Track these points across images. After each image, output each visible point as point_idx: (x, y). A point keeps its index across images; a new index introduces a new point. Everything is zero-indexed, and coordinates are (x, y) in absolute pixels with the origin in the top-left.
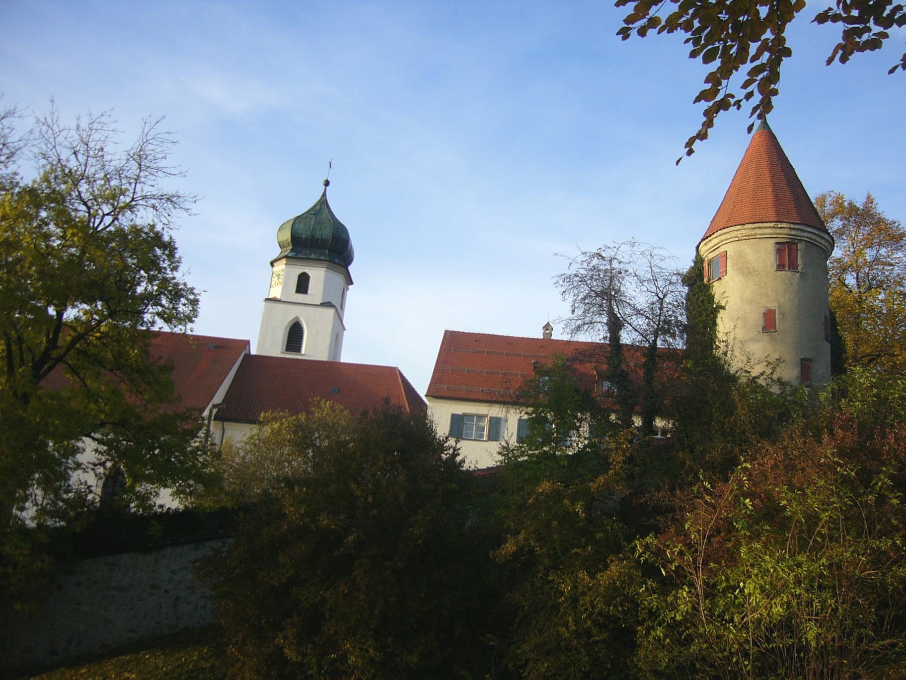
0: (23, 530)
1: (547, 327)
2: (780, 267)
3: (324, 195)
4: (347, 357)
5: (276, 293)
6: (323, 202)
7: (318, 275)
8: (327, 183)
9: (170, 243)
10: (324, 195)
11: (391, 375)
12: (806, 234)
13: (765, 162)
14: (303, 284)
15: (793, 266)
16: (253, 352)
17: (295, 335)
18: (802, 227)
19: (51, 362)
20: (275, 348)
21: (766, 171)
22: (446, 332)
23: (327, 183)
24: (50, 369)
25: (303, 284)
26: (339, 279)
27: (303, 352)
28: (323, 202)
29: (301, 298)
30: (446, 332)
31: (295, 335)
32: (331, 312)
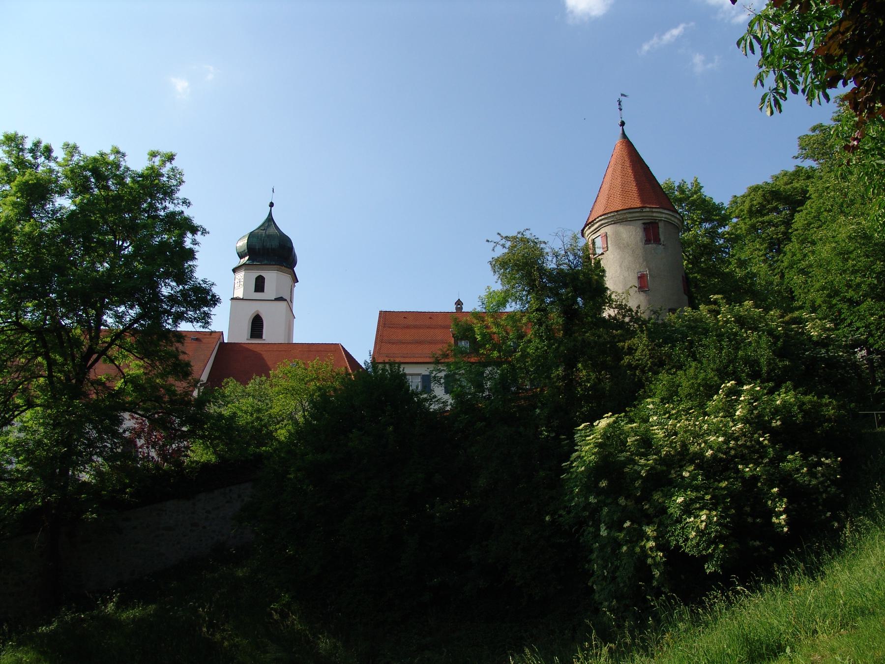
0: (608, 534)
1: (459, 303)
2: (648, 241)
3: (270, 214)
4: (296, 340)
5: (239, 293)
6: (270, 219)
7: (273, 278)
8: (272, 205)
9: (851, 50)
10: (270, 214)
11: (335, 350)
12: (664, 215)
13: (627, 164)
14: (260, 285)
15: (657, 241)
16: (226, 341)
17: (257, 325)
18: (661, 210)
19: (95, 356)
20: (243, 336)
21: (630, 171)
22: (381, 312)
23: (272, 205)
24: (96, 360)
25: (260, 285)
26: (287, 278)
27: (264, 337)
28: (270, 219)
29: (259, 295)
30: (381, 312)
31: (257, 325)
32: (283, 304)
